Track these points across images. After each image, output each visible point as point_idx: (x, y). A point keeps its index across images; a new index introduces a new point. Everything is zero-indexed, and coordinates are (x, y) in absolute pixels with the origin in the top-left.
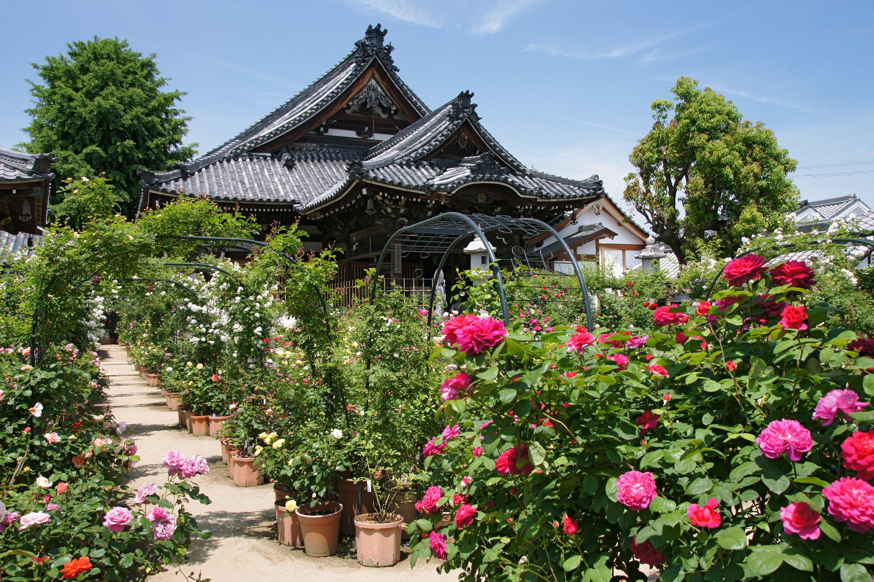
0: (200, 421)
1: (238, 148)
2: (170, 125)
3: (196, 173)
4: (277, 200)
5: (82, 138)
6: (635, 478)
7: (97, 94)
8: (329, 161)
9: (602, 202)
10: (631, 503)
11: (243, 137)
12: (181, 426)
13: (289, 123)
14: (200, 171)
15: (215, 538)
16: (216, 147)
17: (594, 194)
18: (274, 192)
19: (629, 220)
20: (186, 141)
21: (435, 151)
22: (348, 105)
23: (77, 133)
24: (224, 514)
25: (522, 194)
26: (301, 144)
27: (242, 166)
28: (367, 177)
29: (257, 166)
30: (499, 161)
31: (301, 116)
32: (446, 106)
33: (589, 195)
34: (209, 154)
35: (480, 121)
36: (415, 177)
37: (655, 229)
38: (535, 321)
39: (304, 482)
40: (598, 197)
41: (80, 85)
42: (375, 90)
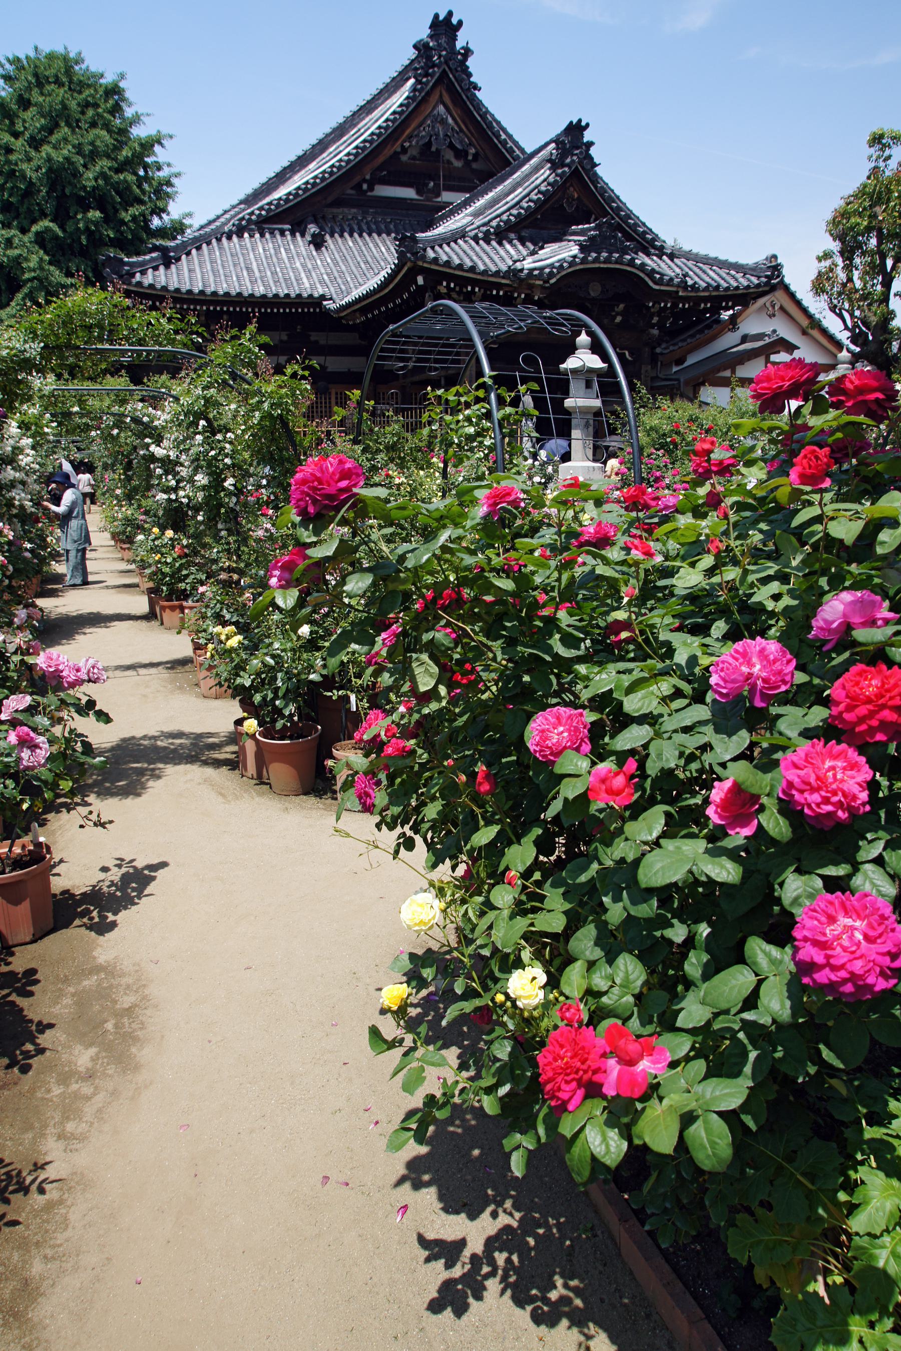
0: (173, 608)
1: (243, 219)
2: (151, 185)
3: (184, 257)
4: (299, 296)
5: (28, 209)
6: (558, 718)
7: (44, 141)
8: (375, 235)
9: (779, 297)
10: (544, 756)
11: (249, 200)
12: (150, 616)
13: (316, 177)
14: (188, 254)
15: (161, 766)
16: (212, 217)
17: (766, 284)
18: (295, 284)
19: (815, 323)
20: (175, 210)
21: (527, 217)
22: (402, 146)
23: (22, 202)
24: (180, 735)
25: (656, 283)
26: (335, 210)
27: (249, 245)
28: (424, 257)
29: (271, 245)
30: (623, 231)
31: (333, 166)
32: (547, 144)
33: (758, 286)
34: (202, 227)
35: (597, 169)
36: (496, 258)
37: (854, 340)
38: (658, 474)
39: (266, 695)
40: (773, 288)
41: (19, 127)
42: (443, 122)
